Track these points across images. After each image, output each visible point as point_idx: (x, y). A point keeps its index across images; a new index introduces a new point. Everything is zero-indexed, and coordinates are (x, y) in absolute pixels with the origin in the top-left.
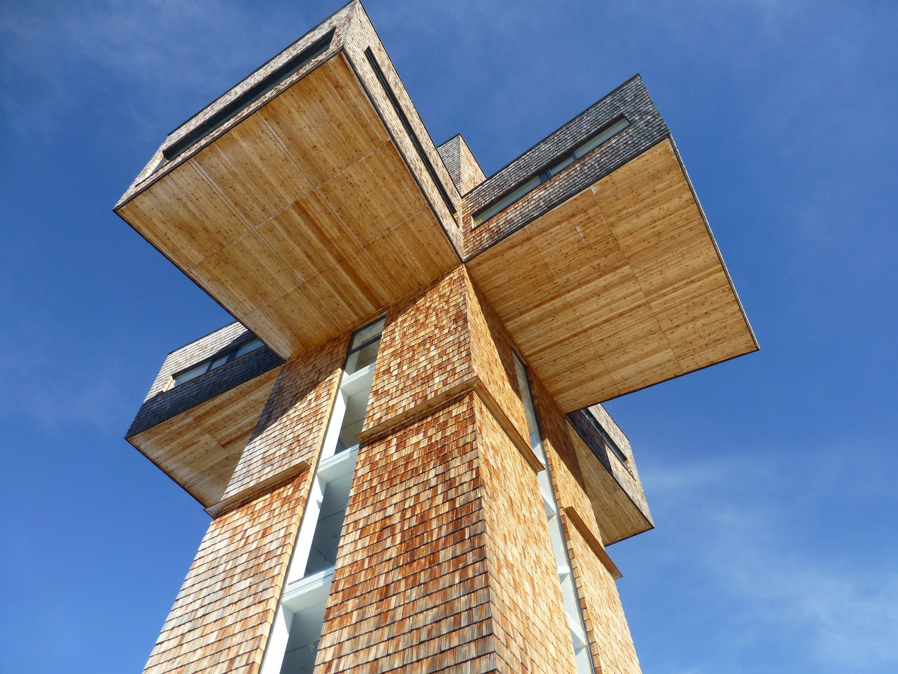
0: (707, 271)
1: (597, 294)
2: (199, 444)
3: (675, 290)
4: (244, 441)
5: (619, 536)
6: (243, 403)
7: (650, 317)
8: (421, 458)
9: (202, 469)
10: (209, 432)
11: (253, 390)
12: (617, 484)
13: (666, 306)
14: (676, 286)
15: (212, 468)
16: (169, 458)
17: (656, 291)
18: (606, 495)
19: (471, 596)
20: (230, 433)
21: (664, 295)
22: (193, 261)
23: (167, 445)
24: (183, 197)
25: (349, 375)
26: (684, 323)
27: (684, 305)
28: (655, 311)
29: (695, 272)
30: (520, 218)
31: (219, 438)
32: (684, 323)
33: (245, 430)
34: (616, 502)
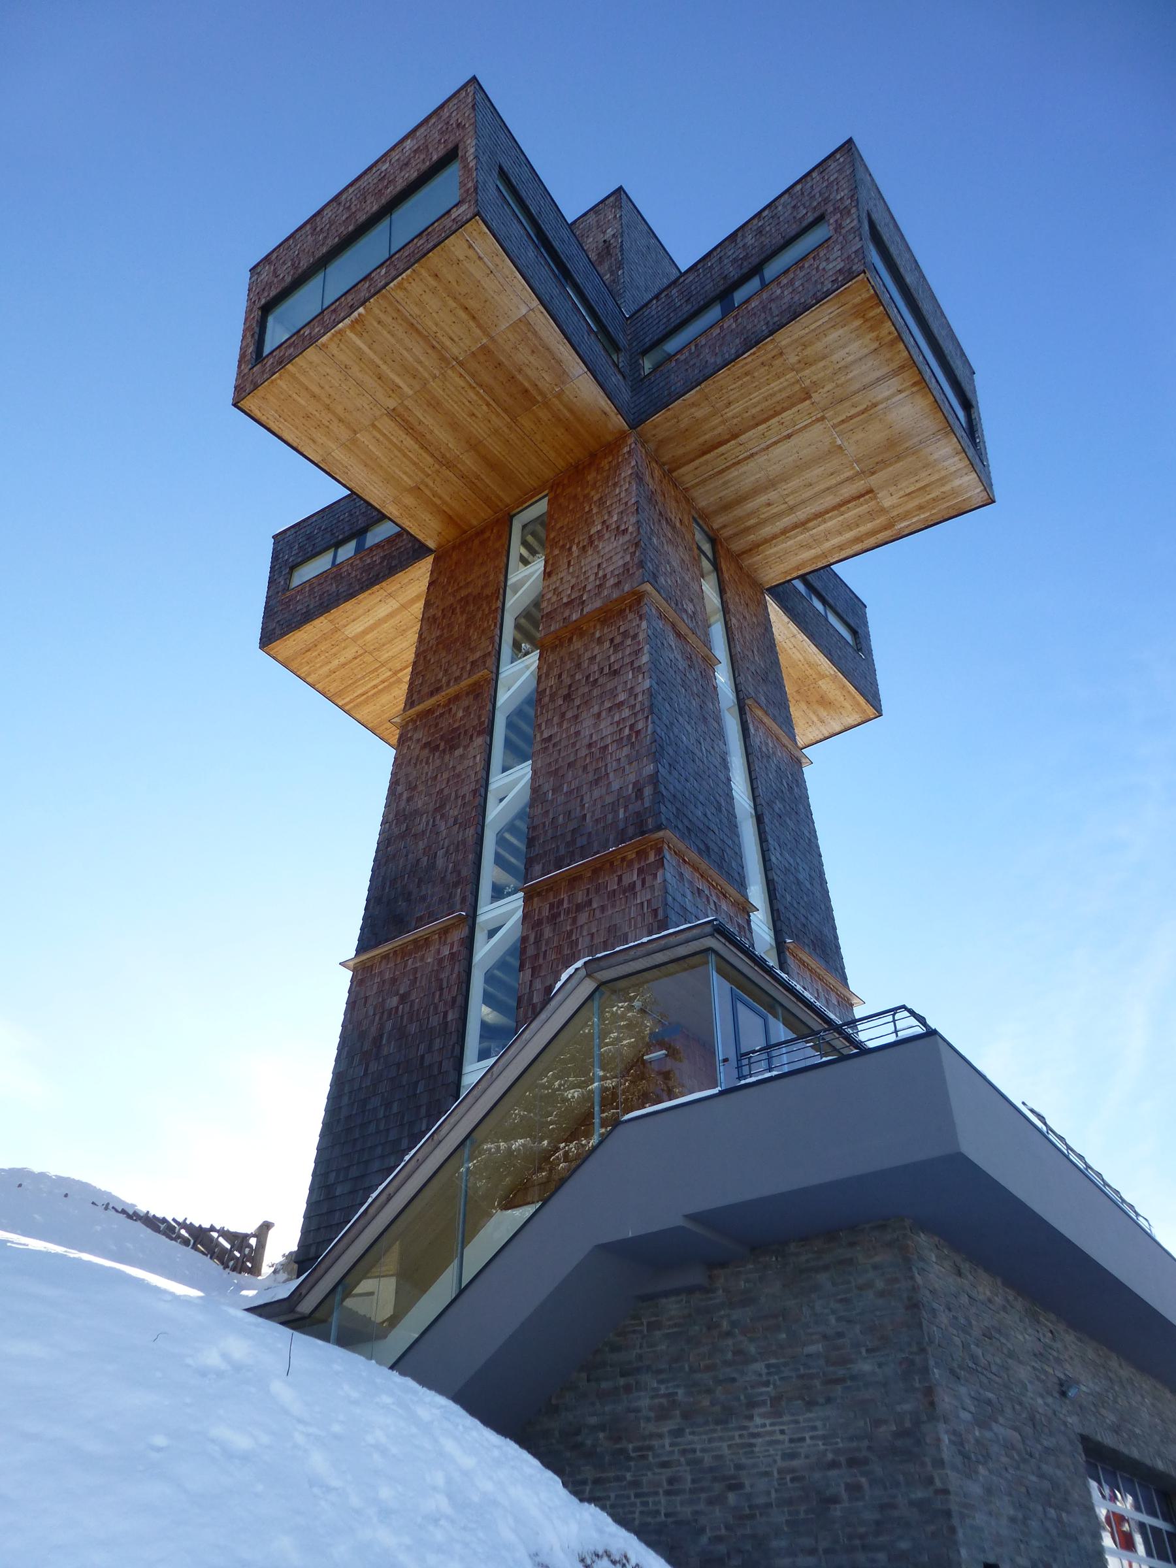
0: (355, 703)
1: (522, 475)
2: (902, 493)
3: (375, 686)
4: (841, 498)
5: (279, 381)
6: (827, 545)
7: (387, 662)
8: (441, 847)
9: (914, 458)
10: (883, 510)
11: (810, 560)
12: (326, 468)
13: (376, 673)
14: (376, 690)
15: (899, 458)
16: (951, 474)
17: (391, 685)
18: (333, 450)
19: (351, 709)
20: (855, 509)
21: (383, 682)
22: (828, 681)
23: (944, 493)
24: (819, 724)
25: (489, 931)
26: (350, 662)
27: (359, 676)
28: (384, 668)
29: (366, 701)
30: (786, 226)
31: (873, 502)
32: (350, 662)
33: (836, 512)
34: (314, 441)
